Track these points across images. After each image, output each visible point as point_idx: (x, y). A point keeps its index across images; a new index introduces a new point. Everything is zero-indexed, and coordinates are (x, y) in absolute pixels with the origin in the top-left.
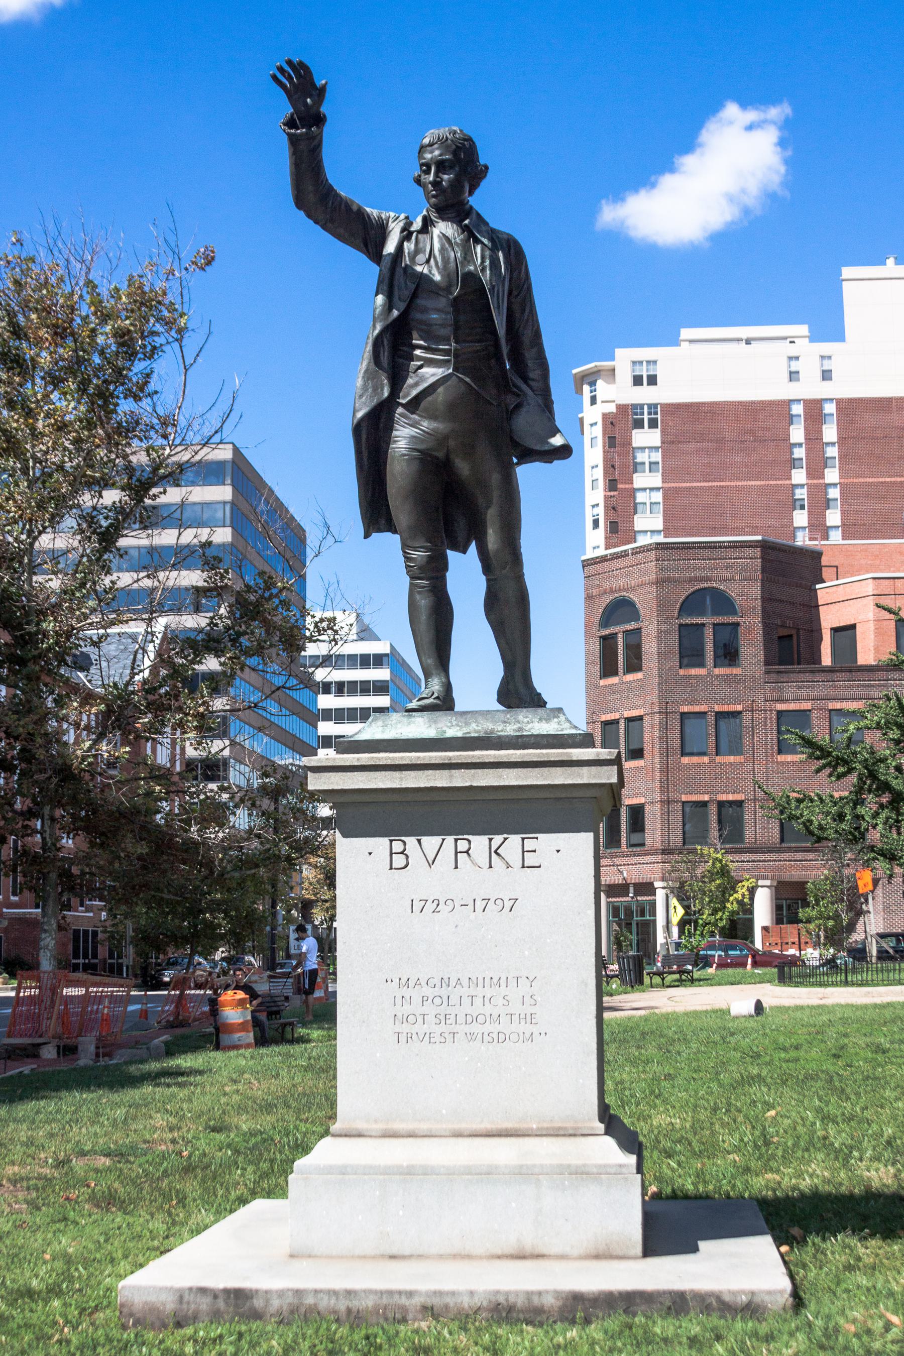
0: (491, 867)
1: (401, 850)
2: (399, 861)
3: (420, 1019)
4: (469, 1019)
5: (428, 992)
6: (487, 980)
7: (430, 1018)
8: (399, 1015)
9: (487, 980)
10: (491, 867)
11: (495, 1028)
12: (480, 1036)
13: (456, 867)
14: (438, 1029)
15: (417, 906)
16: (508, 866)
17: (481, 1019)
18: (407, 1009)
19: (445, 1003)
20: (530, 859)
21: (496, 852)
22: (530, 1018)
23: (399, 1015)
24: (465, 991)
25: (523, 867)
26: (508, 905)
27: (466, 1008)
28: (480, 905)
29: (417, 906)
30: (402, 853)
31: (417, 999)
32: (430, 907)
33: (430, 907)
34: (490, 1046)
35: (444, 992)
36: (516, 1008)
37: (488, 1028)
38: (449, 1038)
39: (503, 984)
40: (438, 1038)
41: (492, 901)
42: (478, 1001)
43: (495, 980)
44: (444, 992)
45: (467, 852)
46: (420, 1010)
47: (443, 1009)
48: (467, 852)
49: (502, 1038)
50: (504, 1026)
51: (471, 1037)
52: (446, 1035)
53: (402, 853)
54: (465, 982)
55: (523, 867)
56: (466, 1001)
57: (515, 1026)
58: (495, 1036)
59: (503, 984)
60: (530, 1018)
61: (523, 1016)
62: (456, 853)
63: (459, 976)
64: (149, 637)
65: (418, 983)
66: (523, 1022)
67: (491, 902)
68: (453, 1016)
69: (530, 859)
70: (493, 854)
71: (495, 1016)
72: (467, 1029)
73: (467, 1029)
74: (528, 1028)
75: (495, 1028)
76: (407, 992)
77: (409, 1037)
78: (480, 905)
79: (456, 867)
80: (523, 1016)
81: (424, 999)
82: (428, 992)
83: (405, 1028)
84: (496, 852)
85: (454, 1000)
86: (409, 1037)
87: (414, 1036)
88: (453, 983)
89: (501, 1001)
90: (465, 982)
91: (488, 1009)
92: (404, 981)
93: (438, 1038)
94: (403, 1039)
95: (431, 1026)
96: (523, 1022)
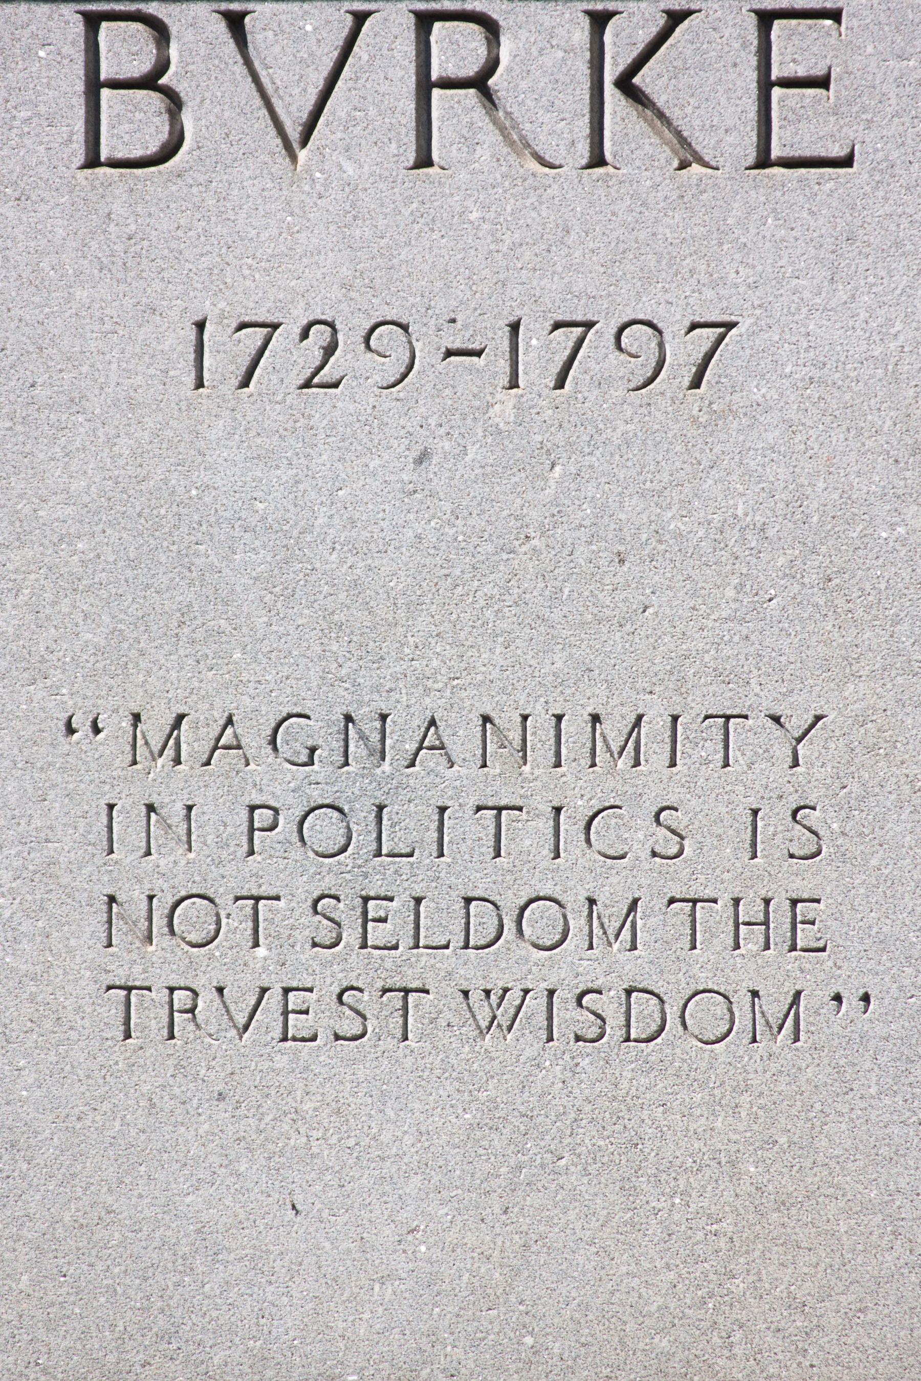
0: (598, 160)
1: (141, 66)
2: (132, 123)
3: (236, 923)
4: (483, 920)
5: (275, 780)
6: (575, 729)
7: (289, 916)
8: (133, 898)
9: (575, 729)
10: (598, 160)
11: (613, 967)
12: (535, 1004)
13: (424, 160)
14: (326, 973)
15: (226, 353)
16: (688, 156)
17: (707, 1014)
18: (172, 870)
19: (363, 841)
20: (800, 124)
21: (625, 84)
22: (791, 923)
23: (133, 898)
24: (460, 781)
25: (763, 161)
26: (684, 351)
27: (470, 865)
28: (541, 351)
29: (226, 353)
30: (149, 82)
31: (220, 818)
32: (290, 357)
33: (290, 357)
34: (588, 1058)
35: (356, 786)
36: (719, 864)
37: (572, 966)
38: (381, 1012)
39: (655, 752)
40: (324, 1017)
41: (606, 329)
42: (528, 835)
43: (614, 730)
44: (356, 786)
45: (479, 82)
46: (234, 876)
47: (346, 876)
48: (479, 82)
49: (642, 1020)
50: (658, 957)
51: (496, 1011)
52: (366, 1000)
53: (149, 82)
54: (463, 738)
55: (763, 161)
56: (468, 831)
57: (711, 962)
58: (609, 1005)
59: (655, 752)
60: (791, 923)
61: (750, 910)
62: (425, 86)
63: (433, 704)
64: (74, 867)
65: (225, 740)
66: (752, 938)
67: (599, 340)
68: (400, 906)
69: (800, 124)
70: (610, 91)
71: (611, 910)
72: (472, 969)
73: (472, 969)
74: (775, 972)
75: (613, 967)
76: (170, 786)
77: (182, 1003)
78: (541, 351)
79: (424, 160)
80: (750, 910)
81: (258, 819)
82: (275, 780)
83: (163, 962)
84: (625, 84)
85: (409, 824)
86: (182, 1003)
87: (207, 1001)
88: (401, 740)
89: (641, 835)
90: (463, 738)
91: (577, 875)
92: (154, 729)
93: (324, 1017)
94: (149, 1014)
95: (287, 953)
96: (752, 938)
